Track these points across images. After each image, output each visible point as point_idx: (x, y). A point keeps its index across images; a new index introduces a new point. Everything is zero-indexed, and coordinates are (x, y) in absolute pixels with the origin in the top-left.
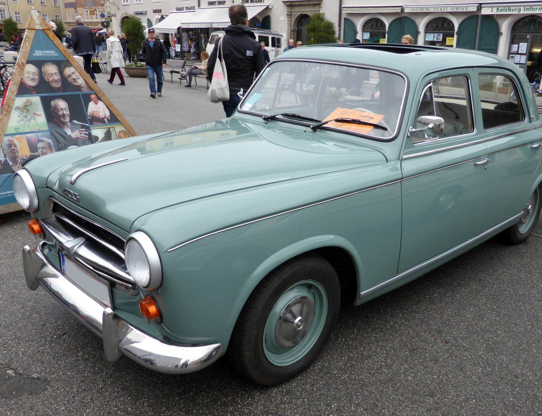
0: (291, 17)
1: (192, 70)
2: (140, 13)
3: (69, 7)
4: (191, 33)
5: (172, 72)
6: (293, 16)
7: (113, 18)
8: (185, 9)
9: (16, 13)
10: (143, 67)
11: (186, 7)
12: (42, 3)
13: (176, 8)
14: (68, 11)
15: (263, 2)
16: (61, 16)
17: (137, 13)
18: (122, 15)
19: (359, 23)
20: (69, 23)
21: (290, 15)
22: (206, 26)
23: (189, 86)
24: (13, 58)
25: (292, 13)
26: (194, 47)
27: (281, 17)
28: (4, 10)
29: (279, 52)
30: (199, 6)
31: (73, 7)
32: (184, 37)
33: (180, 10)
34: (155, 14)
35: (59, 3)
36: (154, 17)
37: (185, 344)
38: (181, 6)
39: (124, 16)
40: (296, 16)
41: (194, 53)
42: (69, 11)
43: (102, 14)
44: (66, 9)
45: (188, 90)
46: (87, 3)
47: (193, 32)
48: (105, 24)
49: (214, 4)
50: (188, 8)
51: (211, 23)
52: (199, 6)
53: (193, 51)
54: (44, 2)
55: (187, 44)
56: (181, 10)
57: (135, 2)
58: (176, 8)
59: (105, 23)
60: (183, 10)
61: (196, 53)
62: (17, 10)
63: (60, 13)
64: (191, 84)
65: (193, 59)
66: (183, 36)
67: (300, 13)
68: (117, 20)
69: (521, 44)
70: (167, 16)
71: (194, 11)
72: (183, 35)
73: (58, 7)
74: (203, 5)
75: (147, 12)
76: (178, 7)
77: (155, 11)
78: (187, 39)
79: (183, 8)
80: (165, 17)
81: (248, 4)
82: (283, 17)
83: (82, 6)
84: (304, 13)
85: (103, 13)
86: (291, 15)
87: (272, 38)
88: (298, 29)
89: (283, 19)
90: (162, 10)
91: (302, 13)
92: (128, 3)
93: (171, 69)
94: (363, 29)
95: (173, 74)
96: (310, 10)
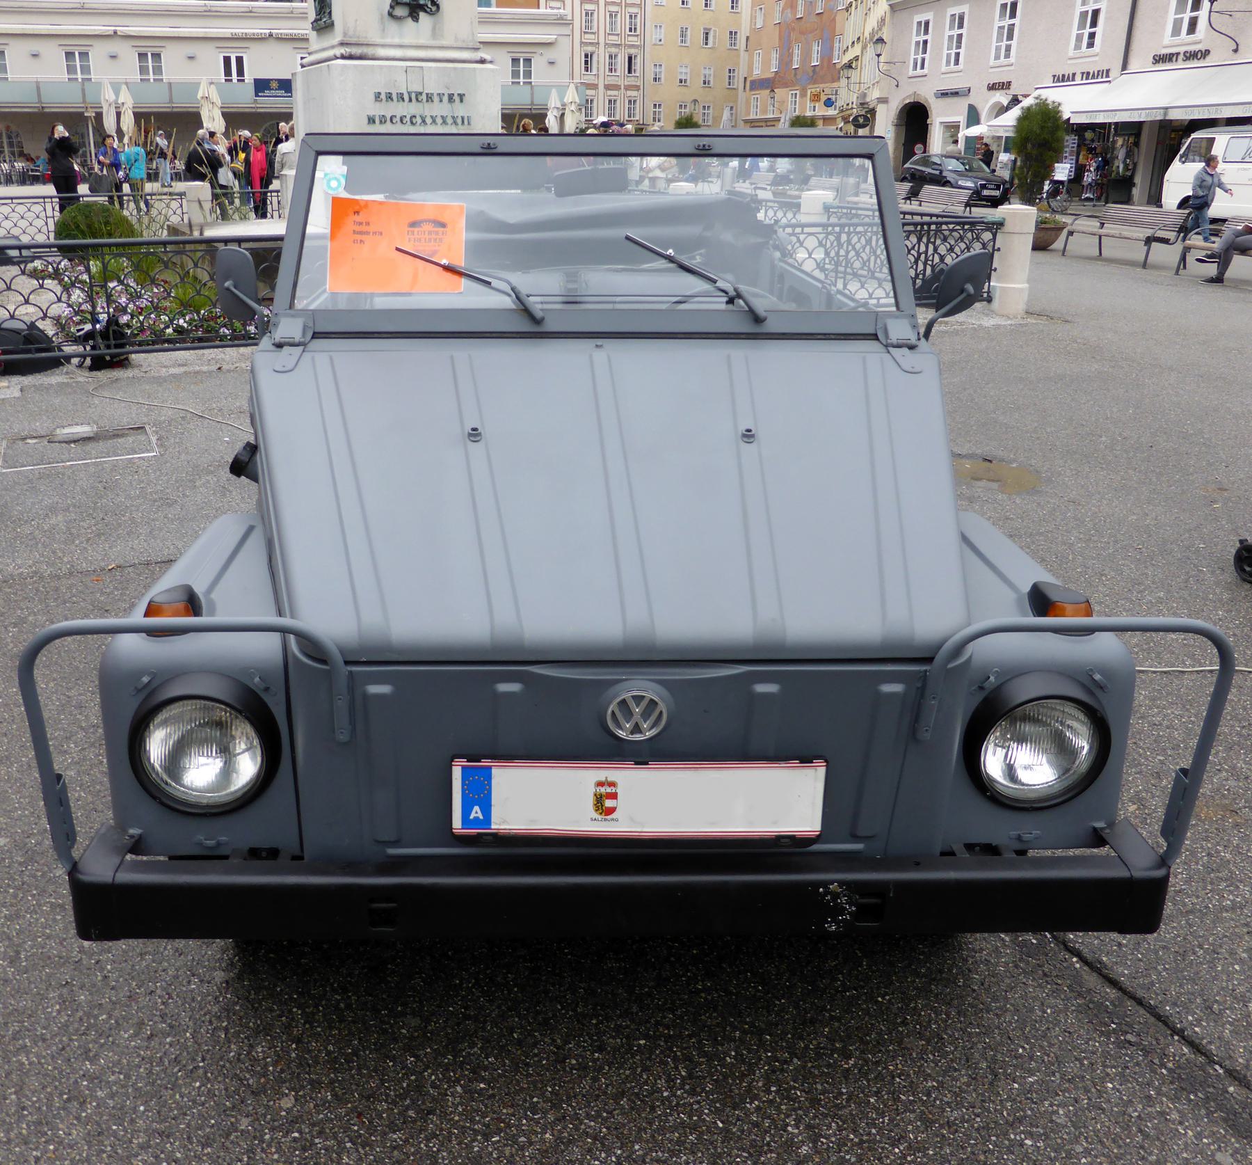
1: (1237, 237)
2: (952, 94)
3: (757, 89)
4: (1089, 135)
5: (1149, 241)
8: (1078, 77)
9: (655, 105)
10: (1045, 223)
11: (1083, 73)
12: (705, 83)
13: (1054, 76)
14: (756, 96)
15: (1176, 60)
16: (736, 109)
17: (942, 94)
18: (904, 99)
20: (766, 122)
22: (1147, 115)
23: (1218, 280)
24: (822, 207)
26: (1097, 169)
28: (635, 101)
29: (736, 173)
30: (1124, 67)
31: (767, 88)
32: (1068, 146)
33: (1063, 81)
34: (992, 92)
35: (738, 82)
36: (987, 101)
37: (286, 656)
38: (1068, 71)
39: (907, 101)
41: (1093, 185)
42: (758, 96)
43: (829, 99)
44: (753, 93)
45: (1215, 291)
46: (798, 77)
47: (1094, 131)
48: (861, 120)
49: (1170, 60)
50: (1088, 73)
51: (1167, 108)
52: (1124, 67)
53: (1090, 180)
54: (709, 81)
55: (1074, 162)
56: (1068, 80)
58: (1054, 76)
59: (860, 119)
60: (1073, 80)
61: (1097, 184)
62: (657, 100)
63: (736, 101)
64: (1223, 274)
65: (1088, 199)
66: (1066, 144)
68: (888, 110)
71: (1109, 81)
72: (1067, 141)
73: (734, 89)
74: (1134, 65)
75: (969, 90)
77: (992, 87)
78: (1075, 149)
79: (1074, 75)
80: (1020, 98)
81: (1171, 64)
83: (785, 85)
85: (830, 96)
87: (237, 57)
90: (1012, 84)
93: (1149, 232)
95: (1154, 244)
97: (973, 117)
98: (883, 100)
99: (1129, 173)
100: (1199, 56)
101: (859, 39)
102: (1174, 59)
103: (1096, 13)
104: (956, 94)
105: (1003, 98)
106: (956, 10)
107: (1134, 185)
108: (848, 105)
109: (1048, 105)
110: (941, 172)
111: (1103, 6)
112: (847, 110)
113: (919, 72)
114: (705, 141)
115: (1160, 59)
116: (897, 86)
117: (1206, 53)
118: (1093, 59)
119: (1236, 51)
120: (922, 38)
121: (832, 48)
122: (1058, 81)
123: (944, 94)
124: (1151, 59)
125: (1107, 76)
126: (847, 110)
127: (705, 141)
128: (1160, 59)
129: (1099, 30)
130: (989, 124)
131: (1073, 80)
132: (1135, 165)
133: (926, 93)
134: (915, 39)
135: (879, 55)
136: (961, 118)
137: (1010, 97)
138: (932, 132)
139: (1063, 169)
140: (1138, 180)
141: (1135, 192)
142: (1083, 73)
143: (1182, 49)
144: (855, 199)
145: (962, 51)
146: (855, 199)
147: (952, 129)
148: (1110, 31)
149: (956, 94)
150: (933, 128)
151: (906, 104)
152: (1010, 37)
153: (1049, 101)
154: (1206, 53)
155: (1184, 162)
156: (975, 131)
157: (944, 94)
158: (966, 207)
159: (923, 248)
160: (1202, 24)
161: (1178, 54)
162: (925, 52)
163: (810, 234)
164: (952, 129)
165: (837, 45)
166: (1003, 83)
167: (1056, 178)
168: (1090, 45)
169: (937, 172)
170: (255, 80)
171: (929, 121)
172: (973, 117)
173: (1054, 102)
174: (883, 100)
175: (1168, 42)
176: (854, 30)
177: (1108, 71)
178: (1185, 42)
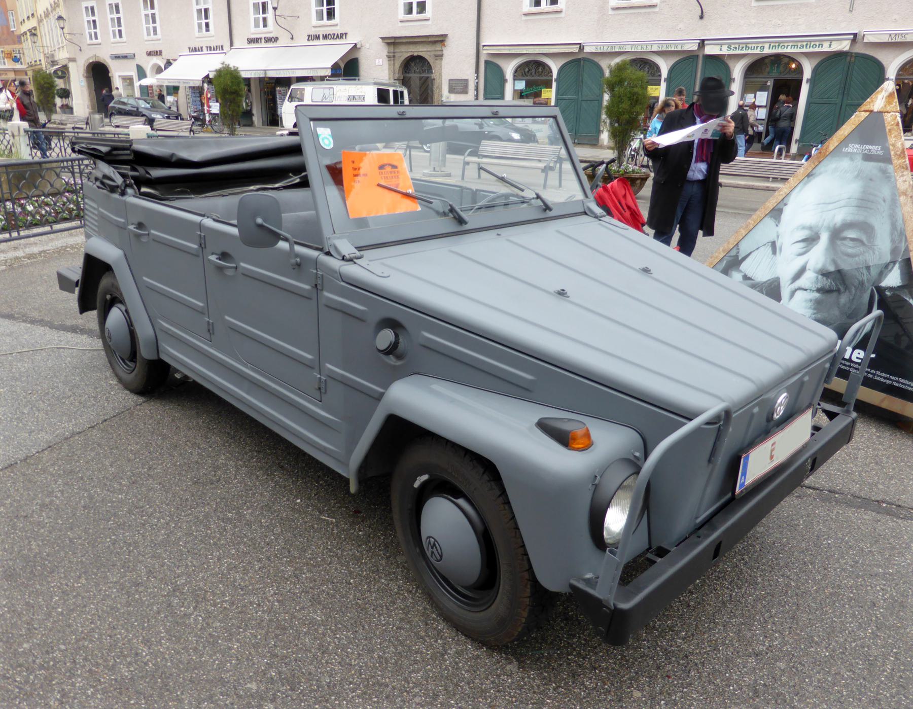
0: (394, 60)
6: (396, 58)
7: (72, 66)
8: (204, 49)
15: (346, 38)
17: (116, 57)
18: (88, 60)
19: (509, 68)
21: (391, 57)
22: (255, 74)
25: (397, 55)
27: (377, 60)
30: (232, 44)
33: (196, 51)
34: (150, 57)
38: (198, 45)
39: (91, 61)
40: (403, 58)
48: (60, 73)
51: (265, 70)
52: (232, 44)
56: (199, 50)
57: (113, 40)
58: (189, 48)
59: (58, 72)
60: (202, 51)
67: (409, 54)
68: (77, 66)
69: (758, 93)
70: (175, 60)
74: (237, 43)
75: (134, 55)
76: (193, 46)
77: (150, 54)
79: (202, 48)
80: (172, 61)
82: (381, 60)
84: (415, 54)
86: (394, 56)
88: (404, 77)
89: (381, 63)
91: (412, 54)
92: (99, 41)
93: (73, 126)
94: (514, 76)
96: (425, 49)
97: (142, 74)
98: (73, 60)
99: (249, 108)
100: (330, 37)
101: (33, 15)
102: (259, 41)
103: (206, 10)
104: (125, 57)
105: (157, 60)
106: (89, 4)
107: (253, 115)
108: (36, 61)
109: (231, 68)
110: (138, 109)
111: (209, 6)
112: (35, 65)
113: (94, 41)
114: (495, 109)
115: (251, 41)
116: (81, 50)
117: (276, 39)
118: (211, 38)
119: (292, 39)
120: (115, 16)
121: (7, 20)
122: (192, 51)
123: (117, 57)
124: (246, 41)
125: (222, 49)
126: (35, 65)
127: (495, 109)
128: (251, 41)
129: (158, 25)
130: (157, 77)
131: (202, 51)
132: (251, 103)
133: (104, 56)
134: (86, 19)
135: (62, 28)
136: (134, 73)
137: (165, 61)
138: (114, 82)
139: (215, 106)
140: (254, 111)
141: (255, 119)
142: (207, 47)
143: (263, 36)
144: (102, 129)
145: (123, 28)
146: (102, 129)
147: (129, 81)
148: (217, 19)
149: (125, 57)
150: (114, 80)
151: (90, 63)
152: (154, 21)
153: (231, 66)
154: (276, 39)
155: (290, 102)
156: (145, 82)
157: (117, 57)
158: (406, 149)
159: (62, 145)
160: (270, 21)
161: (261, 38)
162: (95, 27)
163: (61, 150)
164: (129, 81)
165: (11, 18)
166: (157, 51)
167: (212, 112)
168: (208, 30)
169: (135, 109)
170: (656, 562)
171: (110, 75)
172: (142, 74)
173: (234, 67)
174: (73, 60)
175: (254, 32)
176: (27, 9)
177: (222, 47)
178: (261, 32)
